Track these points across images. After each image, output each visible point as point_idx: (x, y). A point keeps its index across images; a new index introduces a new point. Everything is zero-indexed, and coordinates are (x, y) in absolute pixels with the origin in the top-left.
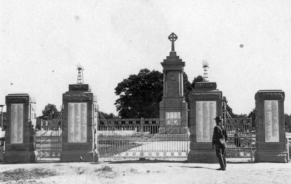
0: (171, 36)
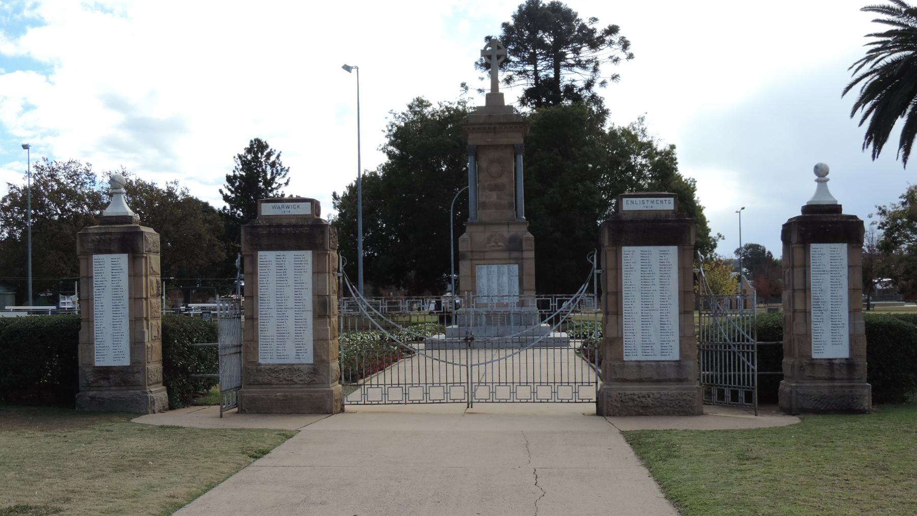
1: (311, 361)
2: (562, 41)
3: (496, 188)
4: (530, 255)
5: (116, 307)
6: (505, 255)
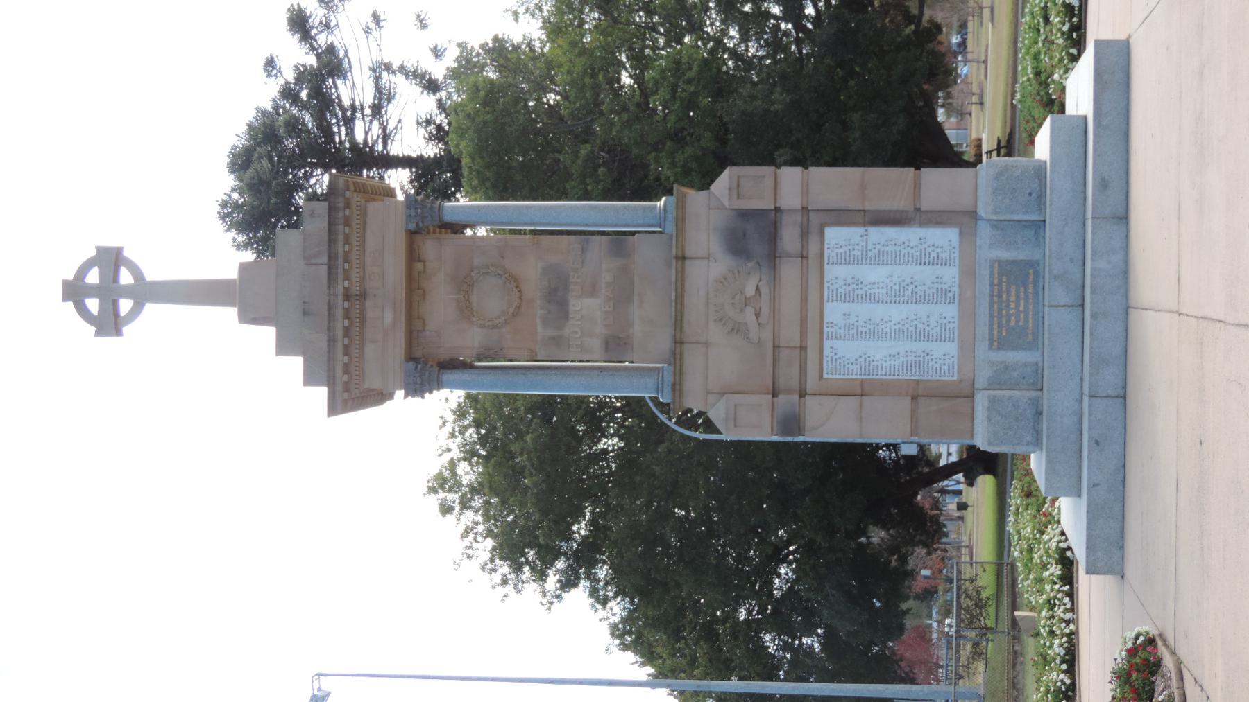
0: (93, 304)
2: (323, 151)
3: (557, 296)
4: (791, 185)
6: (789, 271)
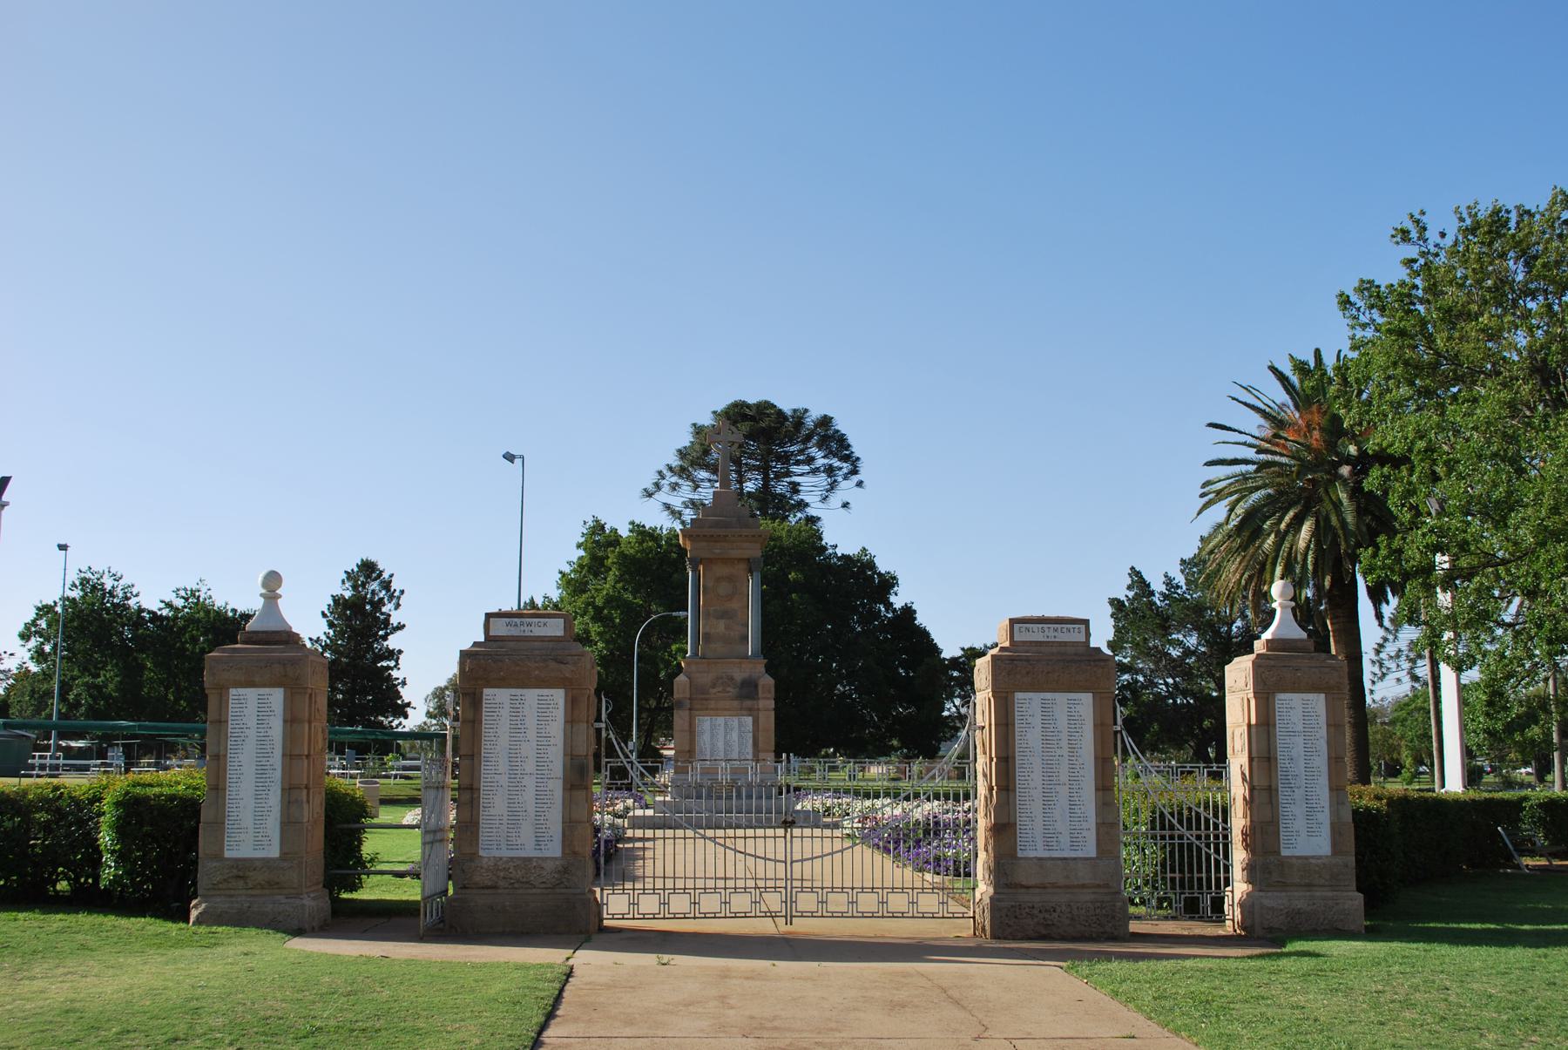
1: (558, 854)
4: (767, 704)
5: (262, 771)
6: (736, 703)
